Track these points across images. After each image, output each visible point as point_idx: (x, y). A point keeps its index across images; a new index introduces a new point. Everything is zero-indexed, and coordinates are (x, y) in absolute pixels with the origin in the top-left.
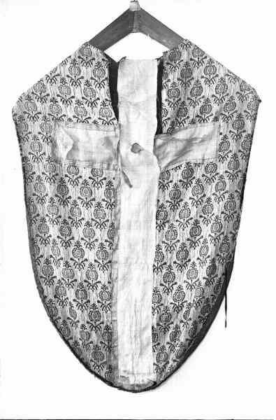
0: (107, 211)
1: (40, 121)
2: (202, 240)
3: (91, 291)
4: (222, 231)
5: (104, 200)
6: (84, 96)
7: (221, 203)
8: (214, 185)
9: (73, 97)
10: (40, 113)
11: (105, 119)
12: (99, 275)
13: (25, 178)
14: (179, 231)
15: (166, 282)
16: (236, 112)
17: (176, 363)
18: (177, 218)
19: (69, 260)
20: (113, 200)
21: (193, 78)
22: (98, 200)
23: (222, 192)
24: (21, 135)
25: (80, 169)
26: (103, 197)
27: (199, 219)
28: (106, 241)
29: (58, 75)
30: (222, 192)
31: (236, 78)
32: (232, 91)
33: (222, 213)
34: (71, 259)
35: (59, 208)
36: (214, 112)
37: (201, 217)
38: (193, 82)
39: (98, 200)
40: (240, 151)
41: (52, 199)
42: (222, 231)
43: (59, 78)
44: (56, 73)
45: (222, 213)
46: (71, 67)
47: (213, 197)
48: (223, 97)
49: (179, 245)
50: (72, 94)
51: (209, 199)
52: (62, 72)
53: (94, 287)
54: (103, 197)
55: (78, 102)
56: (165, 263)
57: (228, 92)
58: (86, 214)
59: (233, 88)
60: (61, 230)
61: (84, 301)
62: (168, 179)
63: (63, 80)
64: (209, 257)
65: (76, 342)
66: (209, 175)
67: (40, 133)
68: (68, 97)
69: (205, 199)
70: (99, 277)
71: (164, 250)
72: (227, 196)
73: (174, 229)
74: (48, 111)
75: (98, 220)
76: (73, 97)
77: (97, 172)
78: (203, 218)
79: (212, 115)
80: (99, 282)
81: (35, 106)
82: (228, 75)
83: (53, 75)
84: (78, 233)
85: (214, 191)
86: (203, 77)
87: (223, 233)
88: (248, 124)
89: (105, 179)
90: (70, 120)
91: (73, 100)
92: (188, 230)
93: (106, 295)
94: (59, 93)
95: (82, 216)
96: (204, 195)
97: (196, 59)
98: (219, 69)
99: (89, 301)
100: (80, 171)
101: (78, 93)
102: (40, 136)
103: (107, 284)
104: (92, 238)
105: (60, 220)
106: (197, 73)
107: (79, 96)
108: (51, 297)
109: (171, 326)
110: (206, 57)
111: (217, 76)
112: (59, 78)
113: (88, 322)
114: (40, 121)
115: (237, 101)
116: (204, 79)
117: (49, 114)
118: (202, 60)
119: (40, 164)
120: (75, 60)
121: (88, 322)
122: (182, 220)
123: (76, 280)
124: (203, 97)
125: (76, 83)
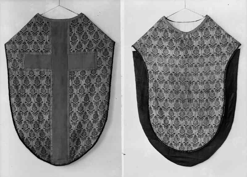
0: (46, 89)
1: (18, 53)
2: (89, 103)
3: (40, 124)
4: (100, 100)
5: (45, 85)
6: (38, 40)
7: (99, 87)
8: (95, 79)
9: (33, 41)
10: (18, 49)
11: (46, 49)
12: (44, 116)
13: (9, 78)
14: (79, 98)
15: (73, 120)
16: (104, 48)
17: (80, 155)
18: (78, 92)
19: (31, 112)
20: (49, 85)
21: (83, 31)
22: (43, 85)
23: (99, 83)
24: (8, 58)
25: (35, 72)
26: (45, 83)
27: (88, 93)
28: (47, 102)
29: (27, 31)
30: (99, 83)
31: (102, 33)
32: (101, 38)
33: (100, 92)
34: (32, 111)
35: (25, 90)
36: (94, 47)
37: (89, 92)
38: (83, 33)
39: (43, 85)
40: (107, 65)
41: (22, 86)
42: (100, 100)
43: (27, 33)
44: (26, 31)
45: (100, 92)
46: (33, 27)
47: (95, 85)
48: (97, 40)
49: (79, 104)
50: (33, 40)
51: (93, 85)
52: (29, 30)
53: (42, 122)
54: (45, 83)
55: (35, 43)
56: (73, 112)
57: (99, 38)
58: (38, 92)
59: (102, 37)
60: (26, 99)
61: (38, 128)
62: (74, 75)
63: (29, 34)
64: (94, 110)
65: (32, 147)
66: (93, 75)
67: (17, 58)
68: (31, 41)
69: (91, 85)
70: (44, 118)
71: (72, 106)
72: (102, 85)
73: (77, 97)
74: (21, 48)
75: (43, 94)
76: (33, 41)
77: (42, 73)
78: (90, 93)
79: (93, 48)
80: (44, 120)
81: (16, 46)
82: (99, 31)
83: (25, 31)
84: (33, 100)
85: (95, 82)
86: (88, 31)
87: (100, 101)
88: (110, 53)
89: (45, 75)
90: (31, 51)
91: (33, 42)
92: (83, 98)
93: (47, 125)
94: (27, 40)
95: (36, 92)
96: (91, 84)
97: (85, 23)
98: (95, 28)
99: (40, 128)
100: (35, 73)
101: (35, 39)
102: (17, 59)
103: (48, 121)
104: (41, 101)
105: (26, 95)
106: (85, 29)
107: (36, 40)
108: (20, 129)
109: (77, 42)
110: (89, 22)
111: (94, 31)
112: (27, 33)
113: (39, 137)
114: (18, 53)
115: (104, 42)
116: (88, 32)
117: (22, 49)
118: (87, 23)
119: (17, 72)
120: (35, 24)
121: (39, 137)
122: (81, 94)
123: (34, 120)
124: (89, 40)
125: (35, 34)
